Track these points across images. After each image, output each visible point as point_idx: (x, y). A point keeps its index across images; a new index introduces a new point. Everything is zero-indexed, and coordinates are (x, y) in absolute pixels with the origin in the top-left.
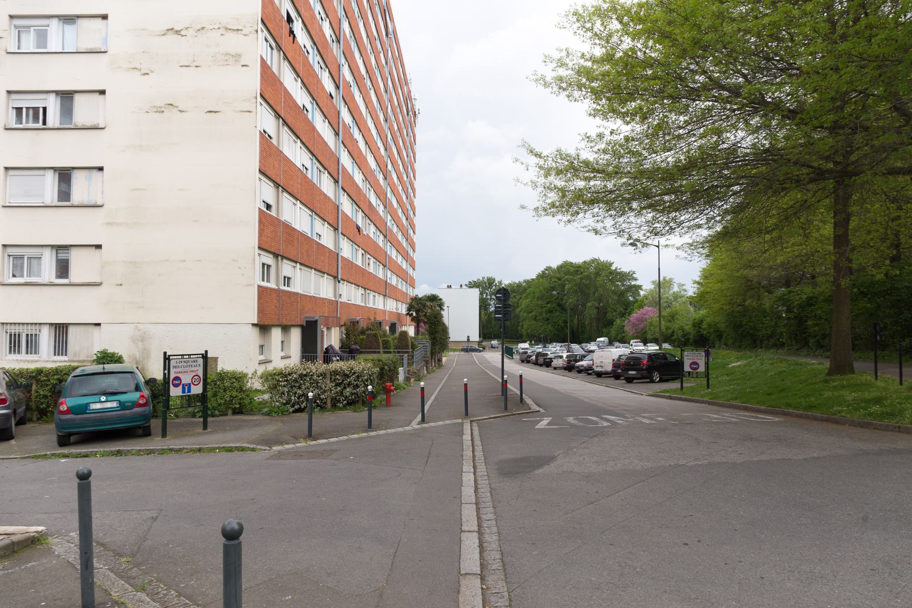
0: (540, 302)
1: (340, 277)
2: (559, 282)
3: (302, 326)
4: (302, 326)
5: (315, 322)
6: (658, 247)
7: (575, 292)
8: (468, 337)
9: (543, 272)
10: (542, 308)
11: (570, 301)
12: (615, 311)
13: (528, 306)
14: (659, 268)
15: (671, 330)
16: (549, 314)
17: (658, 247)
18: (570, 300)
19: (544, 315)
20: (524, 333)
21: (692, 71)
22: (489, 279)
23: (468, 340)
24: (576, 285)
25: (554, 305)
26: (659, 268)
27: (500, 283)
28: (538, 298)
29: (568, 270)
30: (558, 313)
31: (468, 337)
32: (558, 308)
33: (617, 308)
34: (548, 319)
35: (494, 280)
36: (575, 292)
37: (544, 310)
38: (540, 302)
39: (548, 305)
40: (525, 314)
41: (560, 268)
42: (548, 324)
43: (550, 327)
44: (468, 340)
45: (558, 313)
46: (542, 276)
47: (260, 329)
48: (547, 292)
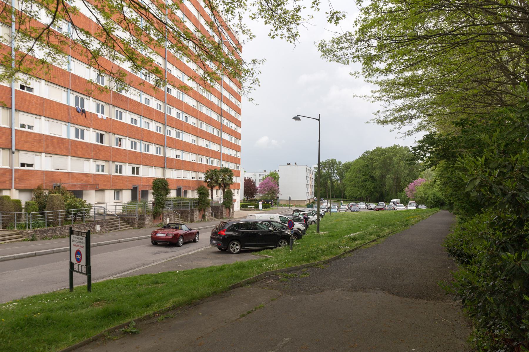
0: (358, 175)
1: (14, 148)
2: (371, 161)
3: (131, 189)
4: (131, 189)
5: (137, 188)
6: (319, 120)
7: (380, 168)
8: (290, 197)
9: (364, 155)
10: (359, 178)
11: (377, 174)
12: (406, 181)
13: (350, 177)
14: (319, 140)
15: (427, 195)
16: (364, 183)
17: (319, 120)
18: (377, 173)
19: (360, 183)
20: (347, 194)
21: (510, 32)
22: (332, 160)
23: (290, 199)
24: (381, 163)
25: (367, 177)
26: (319, 140)
27: (340, 163)
28: (357, 172)
29: (379, 152)
30: (369, 182)
31: (290, 197)
32: (371, 179)
33: (408, 179)
34: (363, 186)
35: (336, 161)
36: (380, 168)
37: (360, 180)
38: (358, 175)
39: (363, 177)
40: (348, 183)
41: (374, 151)
42: (363, 189)
43: (364, 191)
44: (290, 199)
45: (369, 182)
46: (363, 158)
47: (19, 191)
48: (363, 168)
